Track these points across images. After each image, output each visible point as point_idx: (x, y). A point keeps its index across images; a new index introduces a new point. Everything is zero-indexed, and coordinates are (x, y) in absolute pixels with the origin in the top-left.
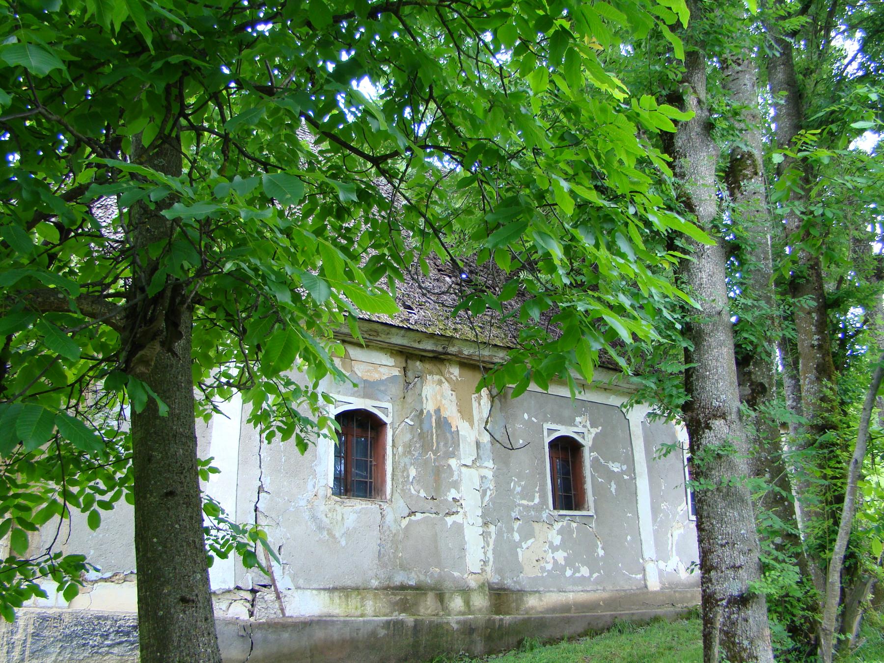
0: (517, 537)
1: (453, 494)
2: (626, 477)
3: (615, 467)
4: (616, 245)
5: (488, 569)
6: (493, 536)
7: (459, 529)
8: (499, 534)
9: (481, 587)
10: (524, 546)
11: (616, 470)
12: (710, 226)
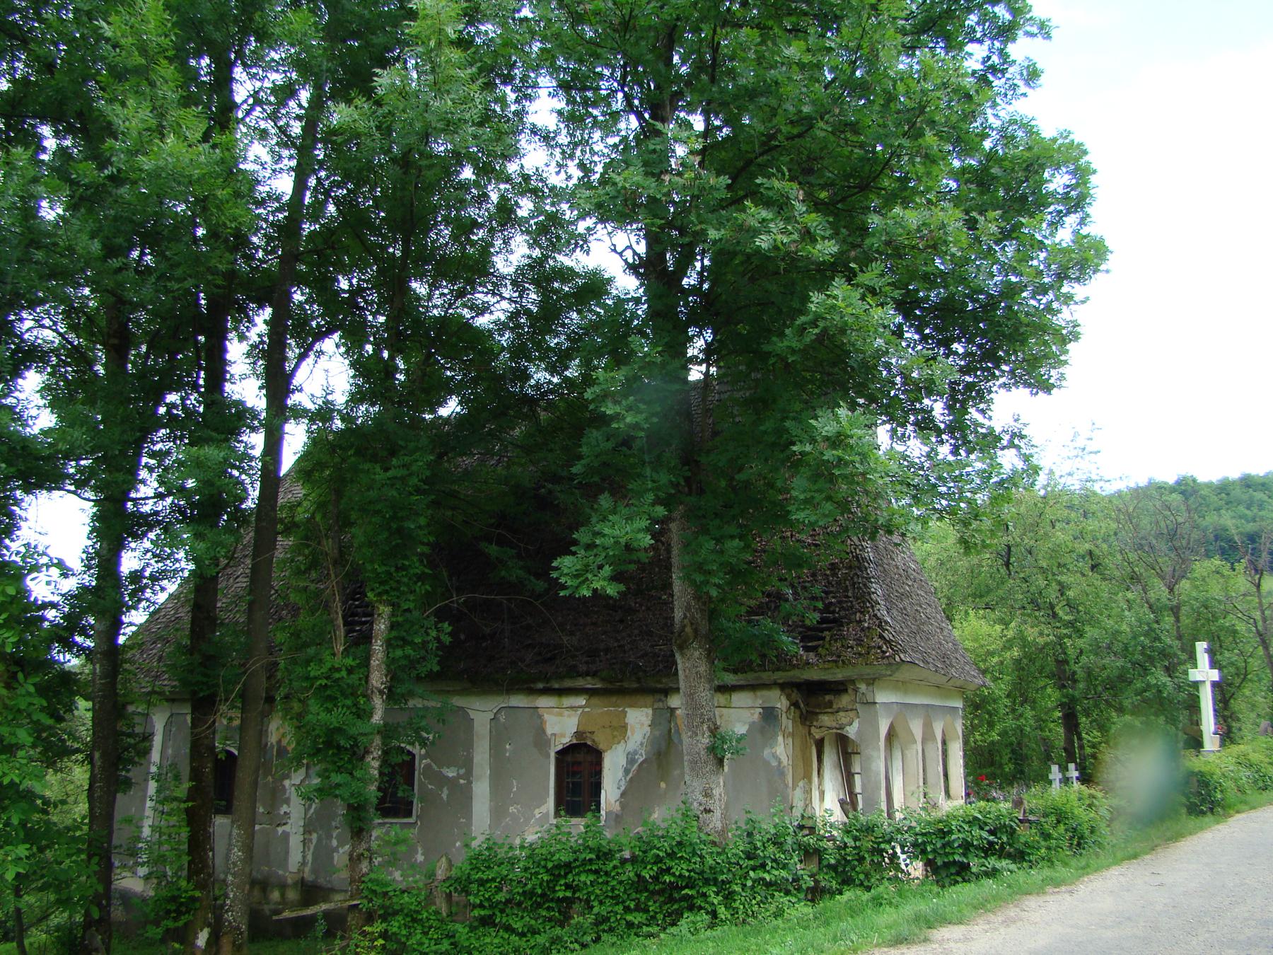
0: (335, 843)
1: (284, 808)
2: (462, 781)
3: (451, 773)
4: (627, 344)
5: (307, 869)
6: (314, 841)
7: (286, 835)
8: (319, 840)
9: (295, 884)
10: (341, 851)
11: (451, 775)
12: (385, 535)
